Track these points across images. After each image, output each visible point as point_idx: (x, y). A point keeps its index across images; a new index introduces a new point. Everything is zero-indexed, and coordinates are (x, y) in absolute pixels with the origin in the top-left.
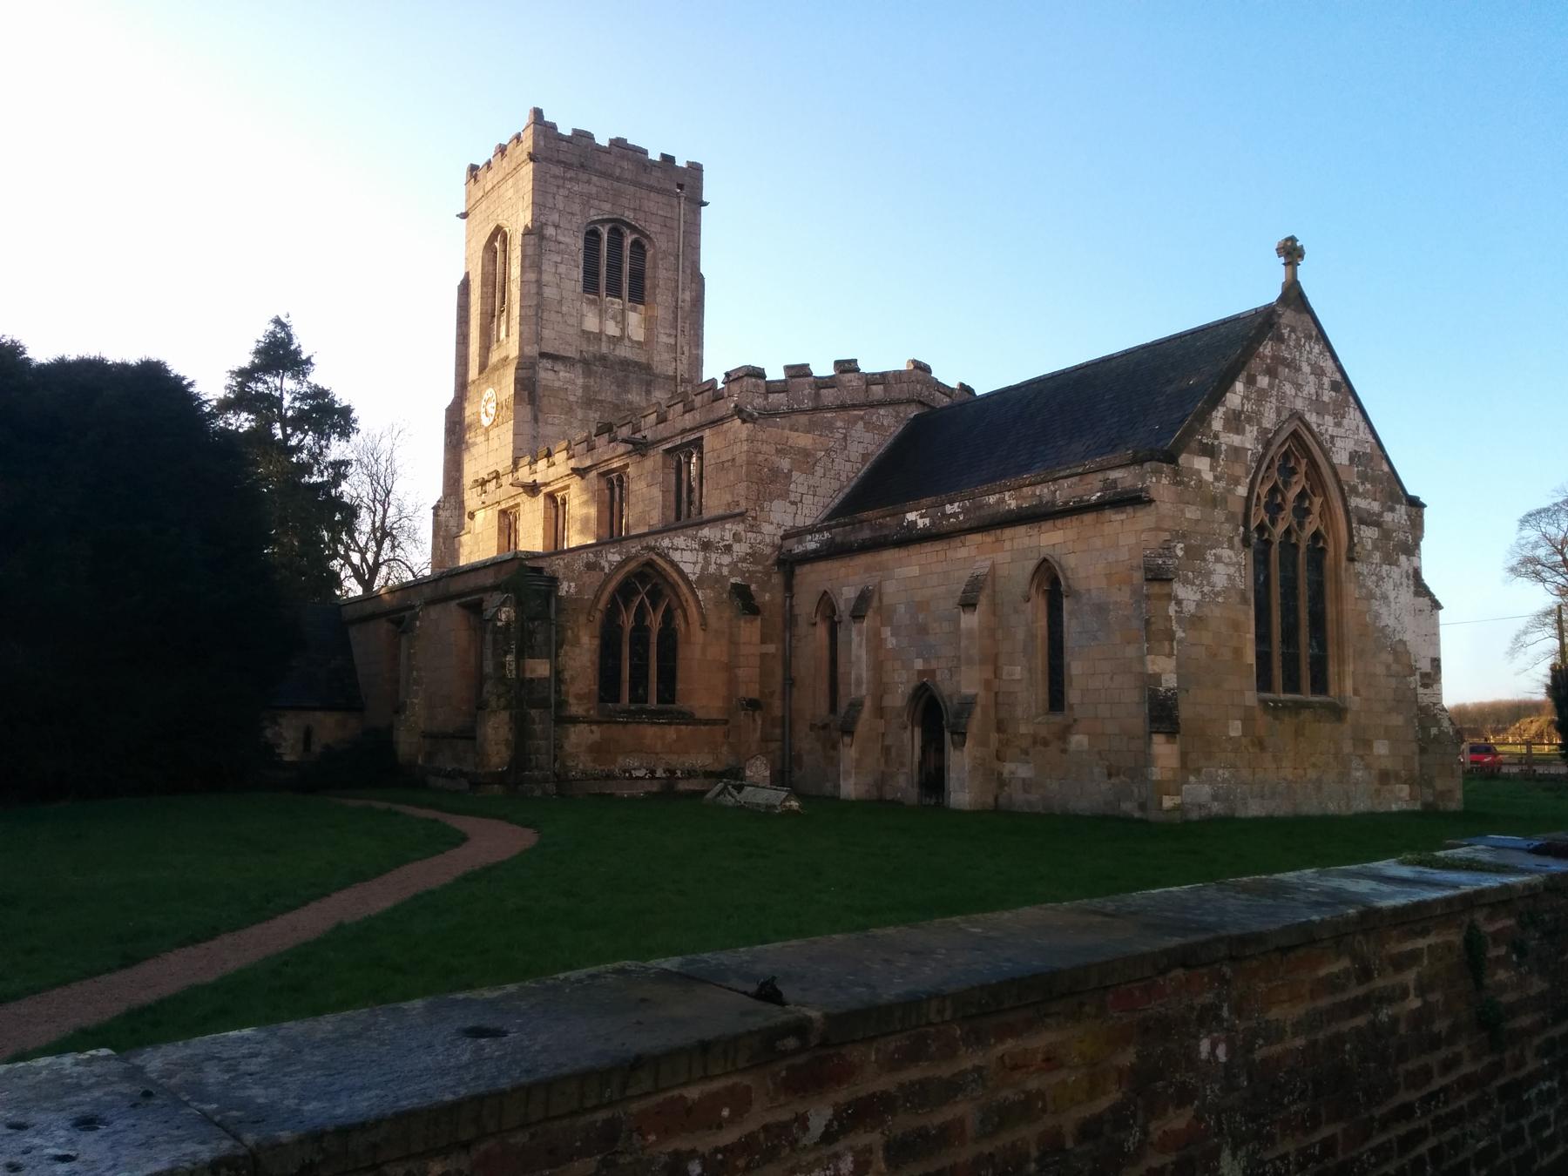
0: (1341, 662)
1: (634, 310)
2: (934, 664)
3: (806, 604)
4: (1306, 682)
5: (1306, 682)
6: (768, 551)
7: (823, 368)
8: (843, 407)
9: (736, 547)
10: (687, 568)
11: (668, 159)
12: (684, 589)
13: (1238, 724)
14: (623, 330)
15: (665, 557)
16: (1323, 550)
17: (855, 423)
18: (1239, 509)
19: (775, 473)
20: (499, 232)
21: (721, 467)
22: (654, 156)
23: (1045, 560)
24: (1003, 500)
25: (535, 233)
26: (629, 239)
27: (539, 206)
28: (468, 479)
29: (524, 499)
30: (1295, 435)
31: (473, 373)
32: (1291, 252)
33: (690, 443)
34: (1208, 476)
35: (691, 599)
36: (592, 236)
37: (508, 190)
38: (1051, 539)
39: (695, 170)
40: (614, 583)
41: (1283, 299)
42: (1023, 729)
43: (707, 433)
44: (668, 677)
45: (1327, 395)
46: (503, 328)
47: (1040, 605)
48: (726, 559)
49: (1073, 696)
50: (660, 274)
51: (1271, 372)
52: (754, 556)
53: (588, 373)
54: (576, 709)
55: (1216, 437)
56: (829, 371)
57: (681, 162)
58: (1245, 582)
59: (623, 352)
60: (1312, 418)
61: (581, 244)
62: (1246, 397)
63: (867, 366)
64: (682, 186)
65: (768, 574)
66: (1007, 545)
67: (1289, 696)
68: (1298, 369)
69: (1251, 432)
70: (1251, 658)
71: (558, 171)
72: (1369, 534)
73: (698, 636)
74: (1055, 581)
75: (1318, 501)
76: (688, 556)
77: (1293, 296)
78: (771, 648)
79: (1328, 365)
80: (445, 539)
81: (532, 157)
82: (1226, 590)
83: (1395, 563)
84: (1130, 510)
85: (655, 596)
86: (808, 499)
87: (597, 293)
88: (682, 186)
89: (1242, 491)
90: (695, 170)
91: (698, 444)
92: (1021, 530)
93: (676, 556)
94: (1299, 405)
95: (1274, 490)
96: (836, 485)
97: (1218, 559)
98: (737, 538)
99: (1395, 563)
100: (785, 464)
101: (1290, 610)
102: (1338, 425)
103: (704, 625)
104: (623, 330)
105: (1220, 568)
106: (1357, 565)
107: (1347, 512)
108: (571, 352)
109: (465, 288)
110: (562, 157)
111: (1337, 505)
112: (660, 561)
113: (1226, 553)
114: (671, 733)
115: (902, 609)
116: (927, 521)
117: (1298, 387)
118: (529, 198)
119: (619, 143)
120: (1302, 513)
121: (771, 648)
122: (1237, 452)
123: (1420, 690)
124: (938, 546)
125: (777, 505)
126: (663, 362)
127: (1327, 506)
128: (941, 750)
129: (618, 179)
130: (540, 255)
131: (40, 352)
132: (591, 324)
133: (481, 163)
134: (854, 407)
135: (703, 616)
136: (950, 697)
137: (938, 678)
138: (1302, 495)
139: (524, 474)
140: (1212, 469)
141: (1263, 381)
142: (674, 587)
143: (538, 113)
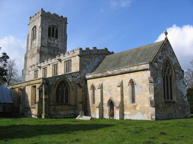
1: (56, 39)
3: (89, 86)
4: (170, 98)
5: (170, 98)
6: (83, 77)
7: (91, 48)
8: (94, 55)
9: (78, 77)
10: (70, 80)
11: (62, 16)
12: (70, 84)
13: (161, 105)
14: (54, 42)
16: (171, 78)
17: (96, 57)
18: (161, 71)
19: (84, 65)
20: (35, 27)
21: (75, 64)
23: (132, 79)
24: (124, 70)
26: (55, 29)
28: (28, 65)
29: (39, 69)
30: (168, 60)
33: (69, 60)
34: (157, 66)
35: (70, 85)
36: (50, 28)
37: (37, 21)
38: (132, 76)
39: (66, 18)
40: (58, 83)
41: (165, 40)
42: (128, 106)
43: (72, 58)
45: (171, 54)
47: (130, 86)
48: (76, 79)
49: (136, 100)
52: (80, 78)
53: (49, 49)
54: (52, 103)
55: (158, 60)
56: (85, 49)
57: (64, 17)
58: (162, 83)
59: (54, 46)
60: (170, 58)
61: (48, 29)
62: (161, 54)
63: (98, 48)
64: (64, 21)
65: (82, 81)
66: (125, 77)
67: (171, 100)
68: (168, 50)
69: (162, 59)
70: (163, 94)
72: (178, 75)
73: (72, 92)
74: (133, 82)
75: (171, 70)
76: (70, 78)
78: (83, 93)
79: (171, 50)
80: (24, 75)
81: (41, 16)
82: (160, 84)
83: (180, 80)
84: (146, 71)
86: (89, 69)
87: (50, 36)
88: (64, 21)
89: (161, 69)
90: (66, 18)
91: (71, 60)
92: (127, 74)
93: (68, 78)
94: (168, 55)
95: (165, 69)
96: (93, 67)
97: (159, 79)
98: (78, 75)
99: (180, 80)
102: (173, 59)
103: (73, 90)
104: (54, 42)
105: (159, 80)
106: (176, 80)
107: (175, 72)
109: (28, 35)
110: (45, 16)
111: (173, 71)
112: (66, 79)
113: (160, 78)
114: (68, 107)
115: (106, 87)
116: (111, 73)
117: (168, 53)
118: (40, 22)
120: (169, 72)
121: (83, 93)
122: (160, 62)
123: (184, 99)
124: (113, 77)
125: (84, 70)
128: (113, 110)
129: (54, 19)
133: (32, 16)
134: (96, 55)
135: (73, 88)
136: (115, 101)
137: (113, 98)
138: (169, 69)
139: (39, 65)
140: (157, 65)
141: (163, 52)
142: (68, 83)
143: (42, 9)
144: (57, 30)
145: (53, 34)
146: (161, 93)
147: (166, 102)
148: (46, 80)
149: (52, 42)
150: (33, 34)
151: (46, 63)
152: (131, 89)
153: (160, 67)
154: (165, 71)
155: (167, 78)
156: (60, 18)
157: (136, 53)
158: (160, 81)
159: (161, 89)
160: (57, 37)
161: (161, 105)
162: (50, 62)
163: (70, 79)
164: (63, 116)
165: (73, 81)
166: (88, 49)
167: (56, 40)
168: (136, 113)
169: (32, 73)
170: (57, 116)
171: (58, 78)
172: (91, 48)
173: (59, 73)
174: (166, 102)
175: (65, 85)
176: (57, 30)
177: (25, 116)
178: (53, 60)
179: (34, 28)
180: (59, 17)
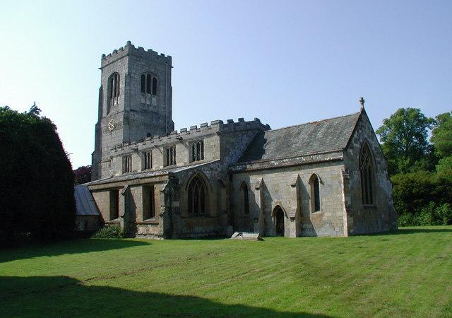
0: (376, 196)
2: (281, 200)
4: (369, 202)
5: (369, 202)
11: (163, 55)
15: (202, 172)
22: (159, 54)
25: (129, 76)
26: (152, 78)
27: (130, 68)
30: (366, 143)
31: (104, 114)
32: (362, 101)
36: (143, 77)
39: (170, 58)
44: (203, 206)
46: (116, 102)
50: (161, 87)
51: (361, 129)
52: (222, 172)
59: (151, 109)
63: (246, 120)
64: (166, 62)
70: (361, 196)
71: (134, 58)
72: (379, 166)
77: (363, 111)
85: (200, 183)
88: (166, 62)
90: (170, 58)
99: (383, 173)
100: (228, 146)
101: (172, 153)
108: (138, 109)
109: (101, 90)
118: (127, 66)
119: (150, 51)
120: (367, 162)
126: (162, 111)
127: (371, 161)
130: (130, 81)
131: (20, 112)
132: (143, 101)
141: (360, 131)
143: (130, 42)
144: (155, 79)
145: (149, 86)
146: (359, 195)
147: (365, 208)
148: (174, 177)
149: (148, 103)
150: (110, 87)
151: (148, 144)
152: (313, 189)
153: (357, 155)
154: (363, 161)
155: (365, 170)
156: (160, 59)
157: (315, 131)
158: (357, 176)
159: (359, 188)
160: (155, 93)
161: (359, 213)
162: (156, 142)
163: (208, 173)
164: (200, 235)
165: (212, 177)
166: (230, 121)
167: (153, 99)
168: (322, 225)
169: (118, 162)
170: (192, 236)
171: (191, 173)
172: (236, 121)
173: (179, 162)
174: (365, 208)
175: (200, 183)
176: (155, 80)
177: (308, 232)
178: (165, 140)
179: (112, 75)
180: (158, 57)
